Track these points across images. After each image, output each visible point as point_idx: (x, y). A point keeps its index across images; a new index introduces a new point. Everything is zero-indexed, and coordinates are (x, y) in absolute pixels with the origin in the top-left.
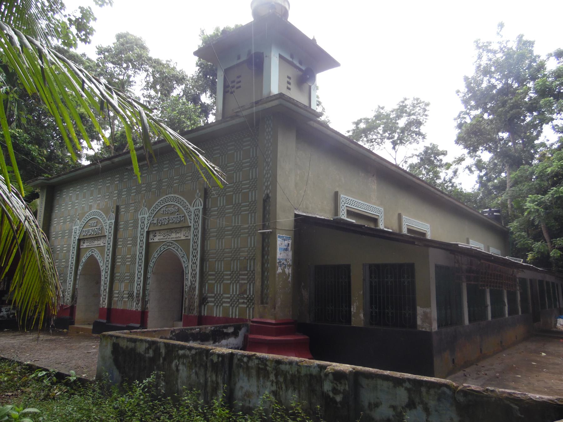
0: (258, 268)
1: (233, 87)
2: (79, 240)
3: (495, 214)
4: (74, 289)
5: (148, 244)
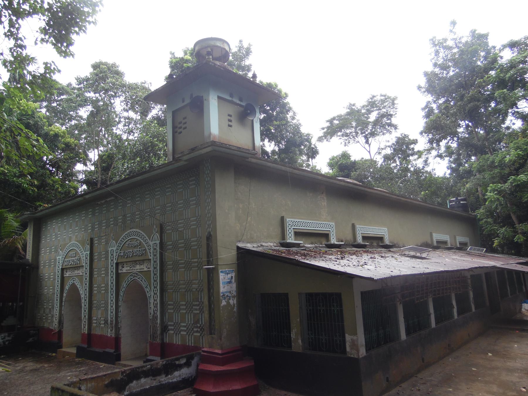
1: (180, 128)
2: (63, 270)
5: (118, 275)
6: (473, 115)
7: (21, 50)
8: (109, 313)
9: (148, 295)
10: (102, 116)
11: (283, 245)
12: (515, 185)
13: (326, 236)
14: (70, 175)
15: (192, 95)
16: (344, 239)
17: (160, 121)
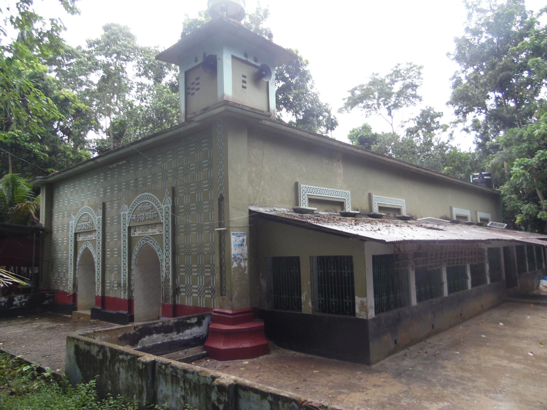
0: (217, 263)
1: (193, 89)
2: (76, 234)
3: (485, 177)
4: (75, 279)
5: (130, 239)
6: (502, 84)
7: (27, 5)
8: (122, 276)
9: (160, 258)
10: (112, 82)
11: (296, 211)
12: (543, 160)
13: (341, 204)
14: (80, 142)
15: (205, 54)
16: (359, 208)
17: (174, 87)
